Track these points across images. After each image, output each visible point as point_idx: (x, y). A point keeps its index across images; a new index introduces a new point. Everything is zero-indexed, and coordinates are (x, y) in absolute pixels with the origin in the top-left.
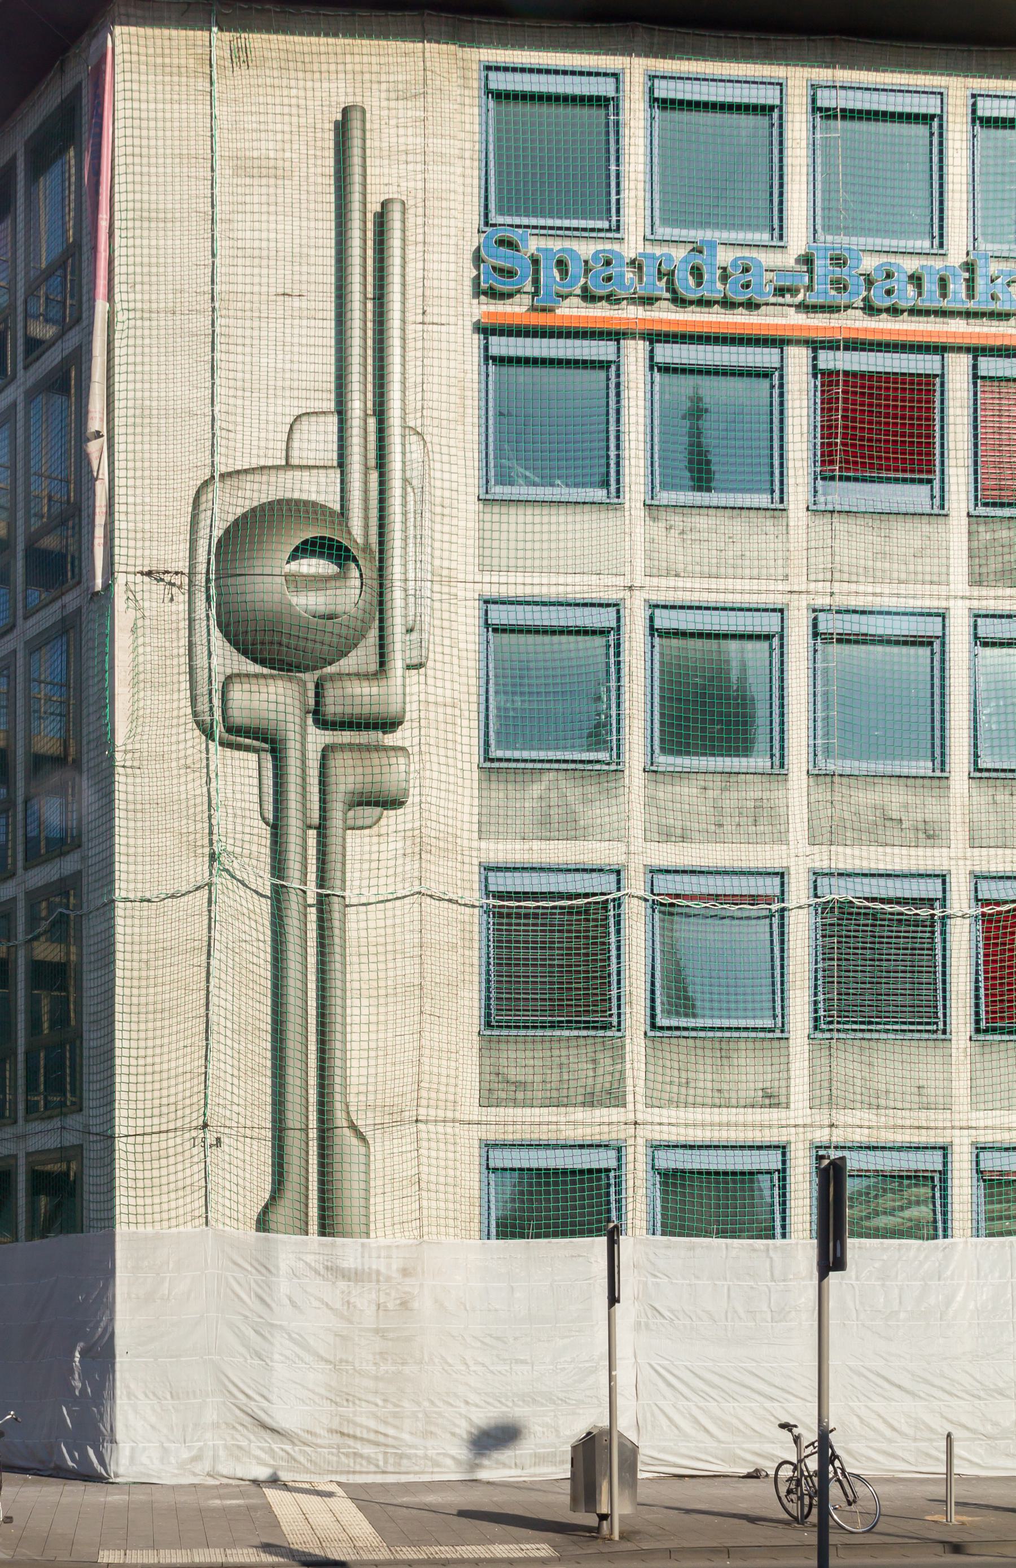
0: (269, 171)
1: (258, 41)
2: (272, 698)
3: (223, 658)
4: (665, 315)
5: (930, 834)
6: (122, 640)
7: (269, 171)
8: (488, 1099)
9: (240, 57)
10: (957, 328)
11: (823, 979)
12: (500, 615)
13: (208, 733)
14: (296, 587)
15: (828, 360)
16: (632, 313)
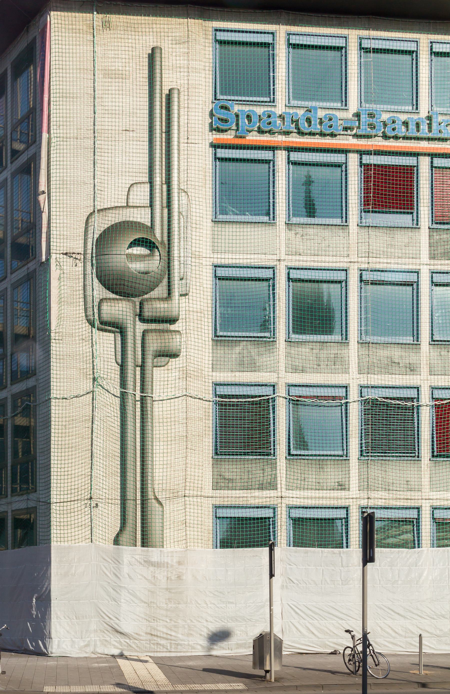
0: (119, 76)
1: (114, 18)
2: (120, 309)
3: (99, 291)
4: (295, 139)
5: (412, 369)
6: (54, 283)
7: (119, 76)
8: (216, 486)
9: (106, 25)
10: (424, 145)
11: (364, 433)
12: (221, 272)
13: (92, 324)
14: (131, 260)
15: (367, 159)
16: (280, 139)
